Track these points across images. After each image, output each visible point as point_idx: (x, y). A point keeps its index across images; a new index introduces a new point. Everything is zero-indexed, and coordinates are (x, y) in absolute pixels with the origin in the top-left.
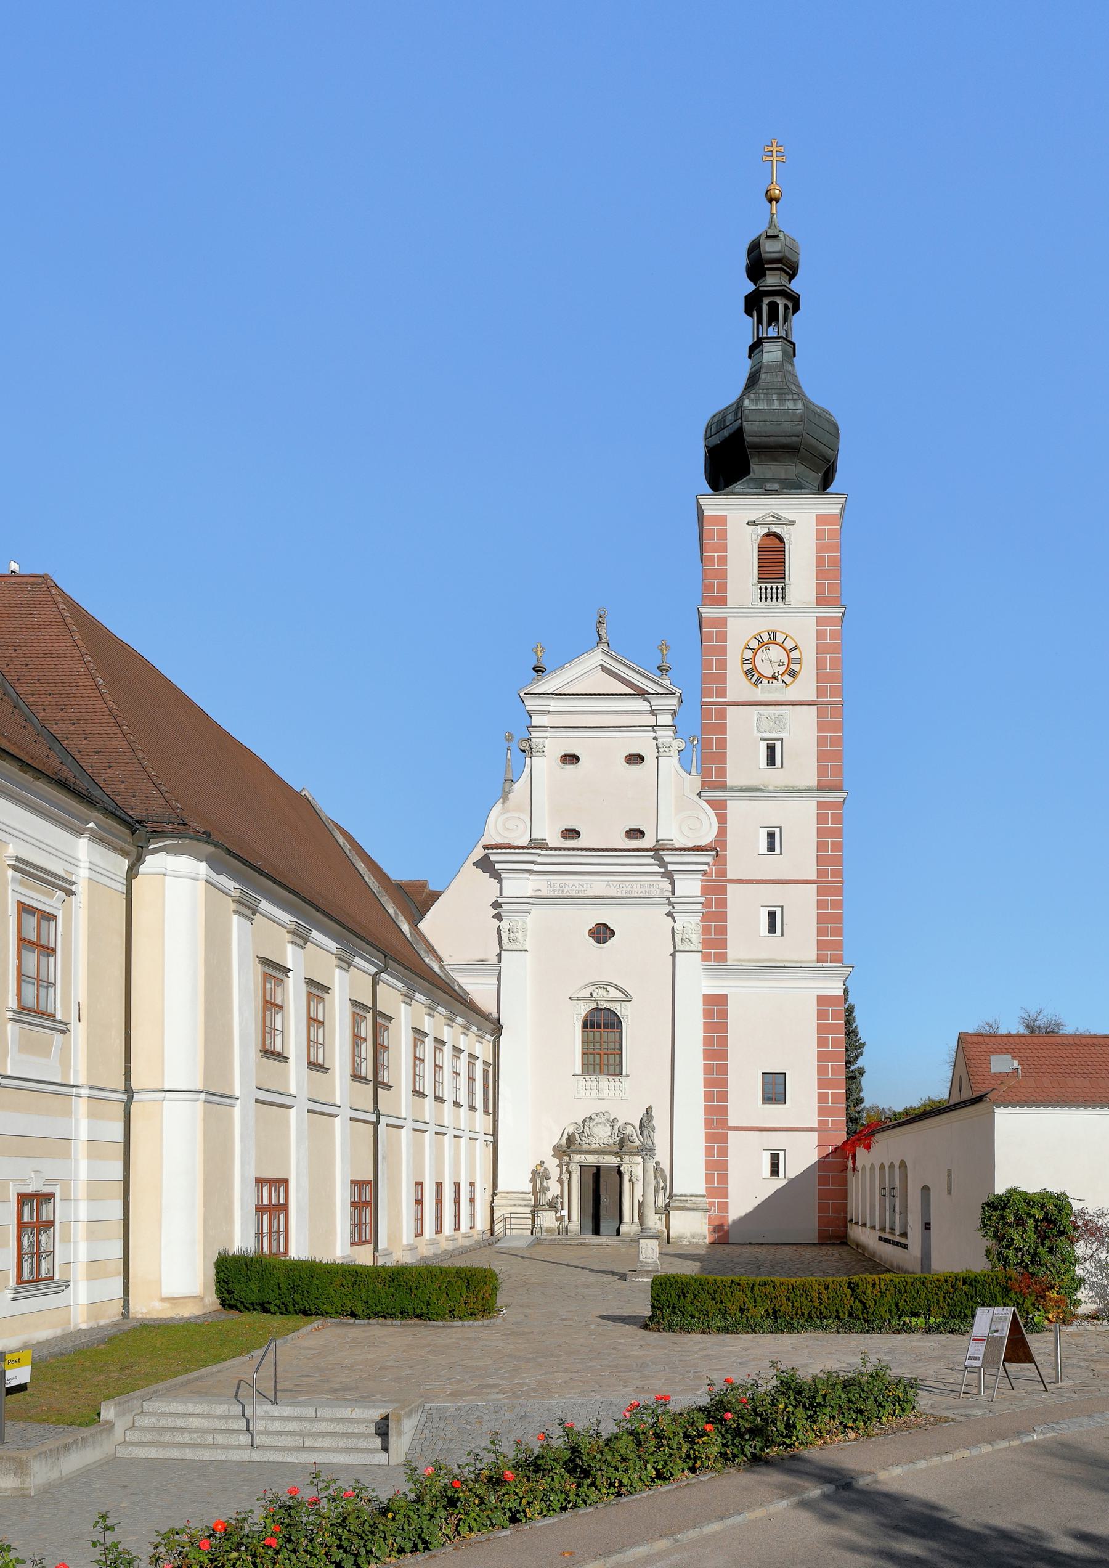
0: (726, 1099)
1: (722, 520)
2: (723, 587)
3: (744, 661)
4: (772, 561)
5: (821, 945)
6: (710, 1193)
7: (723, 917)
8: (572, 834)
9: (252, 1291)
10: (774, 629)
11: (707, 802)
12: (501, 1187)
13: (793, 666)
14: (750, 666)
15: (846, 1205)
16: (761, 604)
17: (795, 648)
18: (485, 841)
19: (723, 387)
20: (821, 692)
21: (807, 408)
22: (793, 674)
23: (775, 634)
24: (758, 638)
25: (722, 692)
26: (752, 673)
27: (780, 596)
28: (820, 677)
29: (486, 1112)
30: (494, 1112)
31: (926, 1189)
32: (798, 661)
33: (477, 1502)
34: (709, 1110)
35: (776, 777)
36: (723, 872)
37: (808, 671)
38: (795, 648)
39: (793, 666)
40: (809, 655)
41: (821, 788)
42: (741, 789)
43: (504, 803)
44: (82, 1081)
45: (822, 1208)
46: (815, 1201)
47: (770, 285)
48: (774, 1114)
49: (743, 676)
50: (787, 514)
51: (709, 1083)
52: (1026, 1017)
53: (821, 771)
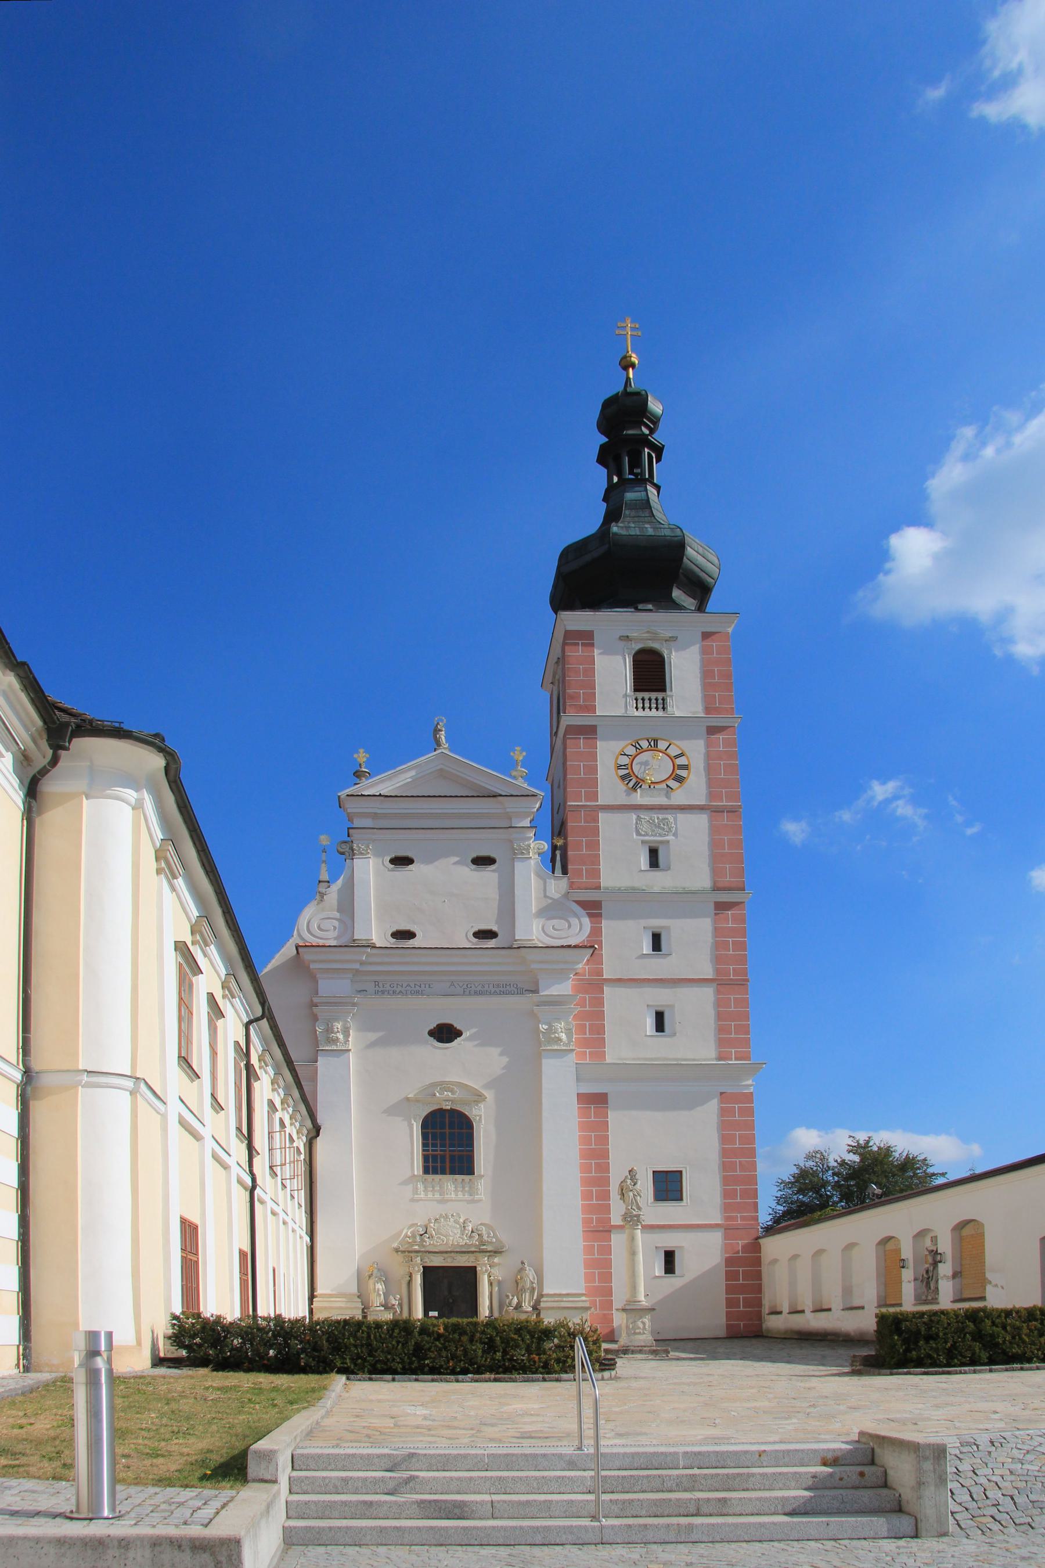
5: (721, 1043)
6: (591, 1292)
7: (601, 1015)
11: (578, 902)
12: (320, 1290)
14: (626, 772)
15: (760, 1299)
16: (636, 714)
17: (682, 755)
19: (585, 519)
20: (711, 795)
22: (680, 779)
25: (594, 796)
26: (631, 780)
28: (710, 783)
32: (685, 767)
33: (379, 1366)
34: (587, 1209)
35: (659, 881)
36: (600, 973)
41: (716, 888)
42: (38, 1514)
45: (730, 1303)
46: (722, 1297)
47: (626, 434)
49: (619, 781)
53: (715, 872)
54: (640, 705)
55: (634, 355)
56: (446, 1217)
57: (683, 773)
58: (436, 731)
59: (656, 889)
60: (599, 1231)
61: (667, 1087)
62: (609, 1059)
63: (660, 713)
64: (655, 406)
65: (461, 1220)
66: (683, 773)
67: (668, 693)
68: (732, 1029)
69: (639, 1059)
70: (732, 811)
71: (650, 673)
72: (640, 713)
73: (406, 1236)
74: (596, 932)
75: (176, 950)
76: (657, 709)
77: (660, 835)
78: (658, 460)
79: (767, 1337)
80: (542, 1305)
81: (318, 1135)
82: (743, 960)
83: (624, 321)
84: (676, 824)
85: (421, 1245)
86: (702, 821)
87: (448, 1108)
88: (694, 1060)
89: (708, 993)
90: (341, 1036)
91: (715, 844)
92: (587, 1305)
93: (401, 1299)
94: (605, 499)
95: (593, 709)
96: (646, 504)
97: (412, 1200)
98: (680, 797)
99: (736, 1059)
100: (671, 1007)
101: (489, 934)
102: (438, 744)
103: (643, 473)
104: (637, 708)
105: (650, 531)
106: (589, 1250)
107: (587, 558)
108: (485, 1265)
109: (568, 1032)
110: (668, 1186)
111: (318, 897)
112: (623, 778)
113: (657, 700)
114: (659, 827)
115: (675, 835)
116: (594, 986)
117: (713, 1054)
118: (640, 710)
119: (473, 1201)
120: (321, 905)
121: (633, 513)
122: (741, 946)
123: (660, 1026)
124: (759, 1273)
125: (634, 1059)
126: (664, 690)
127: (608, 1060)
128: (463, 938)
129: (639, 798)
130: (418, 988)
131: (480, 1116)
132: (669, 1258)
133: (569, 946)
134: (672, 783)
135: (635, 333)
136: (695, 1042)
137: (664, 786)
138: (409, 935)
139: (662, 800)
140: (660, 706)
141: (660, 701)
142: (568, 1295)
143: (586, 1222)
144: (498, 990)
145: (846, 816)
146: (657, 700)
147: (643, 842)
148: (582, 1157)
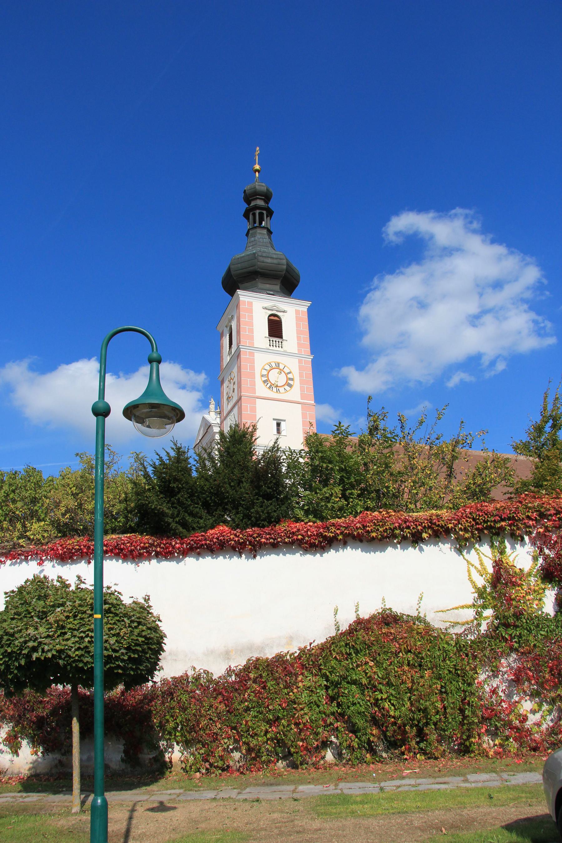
1: (250, 304)
4: (275, 328)
10: (279, 361)
13: (290, 382)
14: (266, 379)
17: (290, 373)
20: (252, 354)
21: (505, 359)
22: (290, 386)
23: (279, 364)
24: (269, 364)
27: (280, 346)
28: (253, 361)
32: (292, 379)
37: (297, 384)
38: (290, 373)
39: (290, 382)
40: (296, 374)
47: (257, 208)
49: (268, 390)
50: (282, 306)
112: (264, 382)
134: (286, 387)
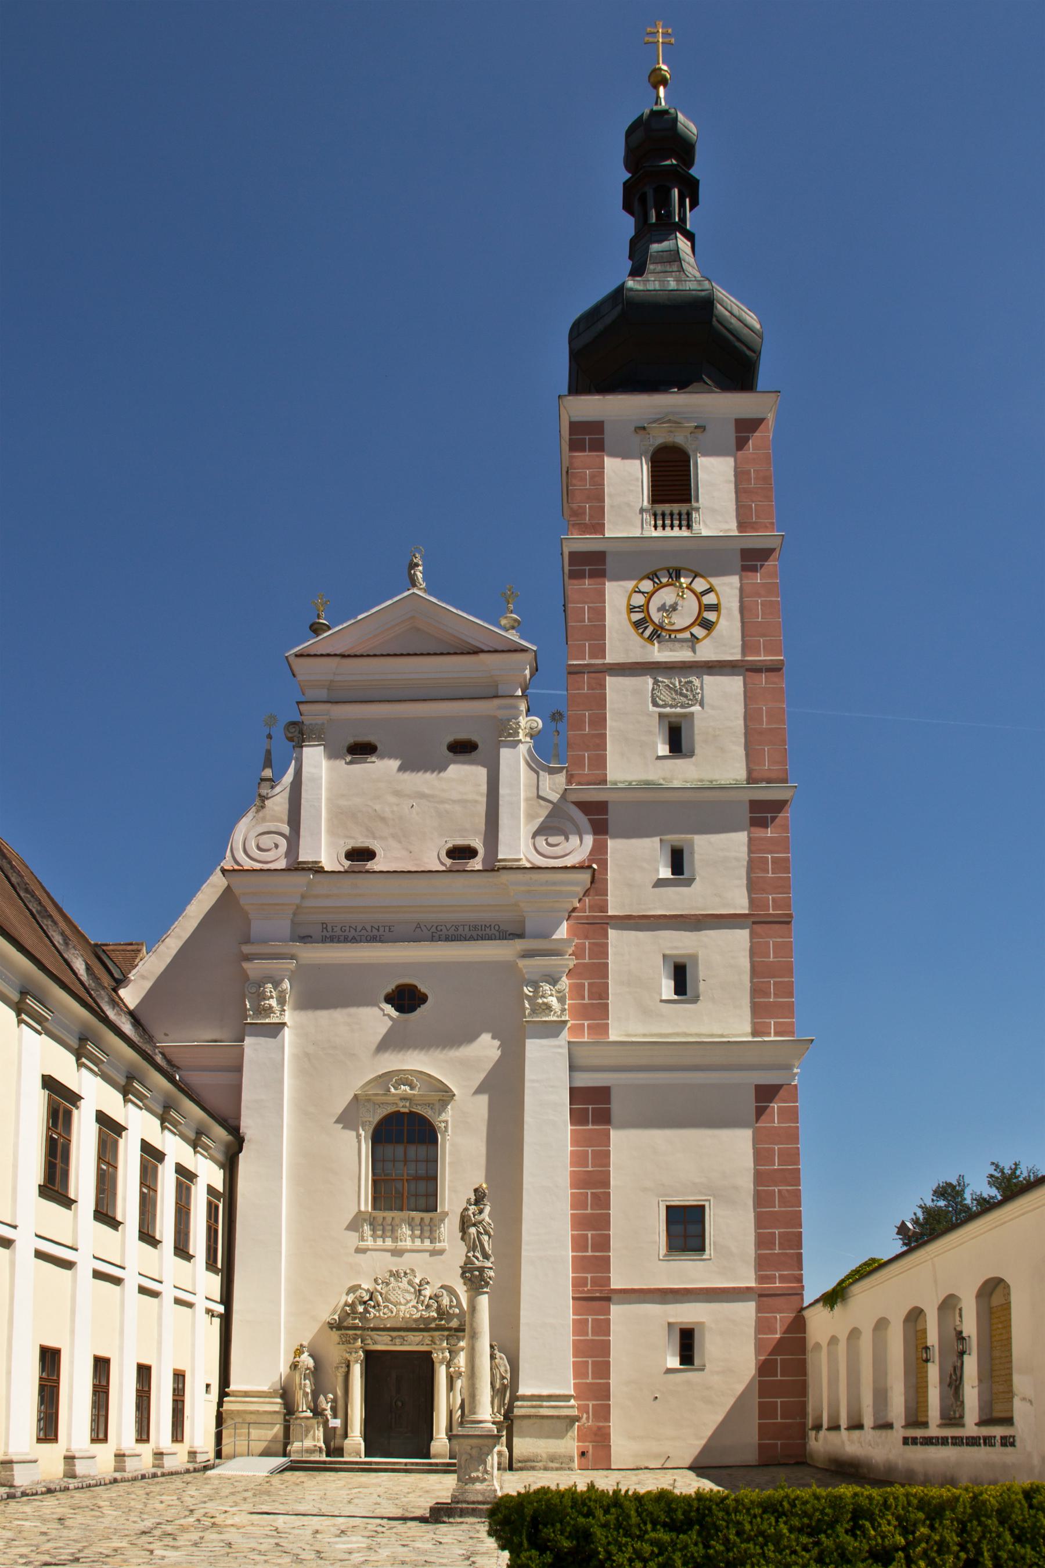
0: (607, 1248)
2: (600, 511)
3: (631, 609)
6: (583, 1392)
8: (360, 855)
9: (144, 1437)
16: (655, 534)
18: (228, 864)
29: (211, 1266)
30: (224, 1264)
31: (179, 1377)
32: (715, 608)
34: (579, 1264)
36: (604, 908)
43: (257, 811)
44: (488, 1418)
47: (659, 171)
48: (689, 1272)
49: (631, 630)
51: (579, 1222)
52: (997, 1174)
54: (659, 523)
55: (664, 67)
56: (396, 1275)
57: (711, 616)
58: (413, 566)
59: (676, 784)
60: (595, 1296)
61: (687, 1090)
62: (614, 1036)
63: (685, 533)
64: (687, 125)
65: (417, 1281)
66: (711, 616)
67: (694, 504)
68: (770, 990)
69: (652, 1035)
70: (774, 669)
71: (672, 483)
72: (659, 533)
73: (346, 1304)
74: (599, 851)
75: (43, 1088)
76: (680, 526)
77: (682, 706)
78: (692, 207)
79: (810, 1465)
80: (517, 1412)
81: (240, 1150)
82: (784, 886)
83: (656, 26)
84: (702, 689)
85: (363, 1317)
86: (735, 684)
87: (406, 1110)
88: (722, 1036)
89: (741, 937)
90: (273, 1002)
91: (750, 716)
92: (575, 1412)
93: (334, 1401)
94: (630, 258)
95: (600, 528)
96: (675, 256)
97: (358, 1251)
98: (706, 652)
99: (777, 1034)
100: (694, 958)
101: (468, 852)
102: (413, 583)
103: (670, 214)
104: (656, 527)
105: (673, 285)
106: (579, 1327)
107: (600, 326)
108: (443, 1350)
109: (561, 1000)
110: (686, 1228)
111: (258, 802)
112: (637, 625)
113: (680, 514)
114: (681, 694)
115: (702, 705)
116: (596, 924)
117: (748, 1028)
118: (660, 529)
119: (434, 1253)
120: (261, 814)
121: (659, 268)
122: (782, 865)
123: (681, 987)
124: (803, 1362)
125: (645, 1035)
126: (689, 501)
127: (614, 1036)
128: (433, 859)
129: (658, 653)
130: (375, 932)
131: (446, 1122)
132: (687, 1344)
133: (566, 868)
134: (699, 632)
135: (666, 40)
136: (723, 1017)
137: (686, 635)
138: (368, 854)
139: (683, 655)
140: (684, 523)
141: (684, 517)
142: (550, 1398)
143: (578, 1283)
144: (474, 934)
145: (674, 162)
146: (680, 514)
147: (661, 716)
148: (573, 1186)
